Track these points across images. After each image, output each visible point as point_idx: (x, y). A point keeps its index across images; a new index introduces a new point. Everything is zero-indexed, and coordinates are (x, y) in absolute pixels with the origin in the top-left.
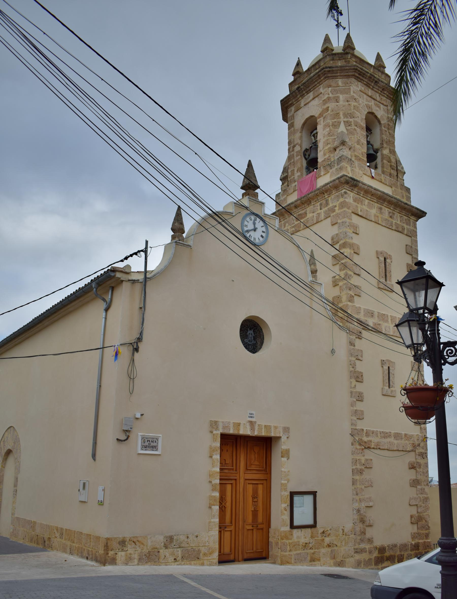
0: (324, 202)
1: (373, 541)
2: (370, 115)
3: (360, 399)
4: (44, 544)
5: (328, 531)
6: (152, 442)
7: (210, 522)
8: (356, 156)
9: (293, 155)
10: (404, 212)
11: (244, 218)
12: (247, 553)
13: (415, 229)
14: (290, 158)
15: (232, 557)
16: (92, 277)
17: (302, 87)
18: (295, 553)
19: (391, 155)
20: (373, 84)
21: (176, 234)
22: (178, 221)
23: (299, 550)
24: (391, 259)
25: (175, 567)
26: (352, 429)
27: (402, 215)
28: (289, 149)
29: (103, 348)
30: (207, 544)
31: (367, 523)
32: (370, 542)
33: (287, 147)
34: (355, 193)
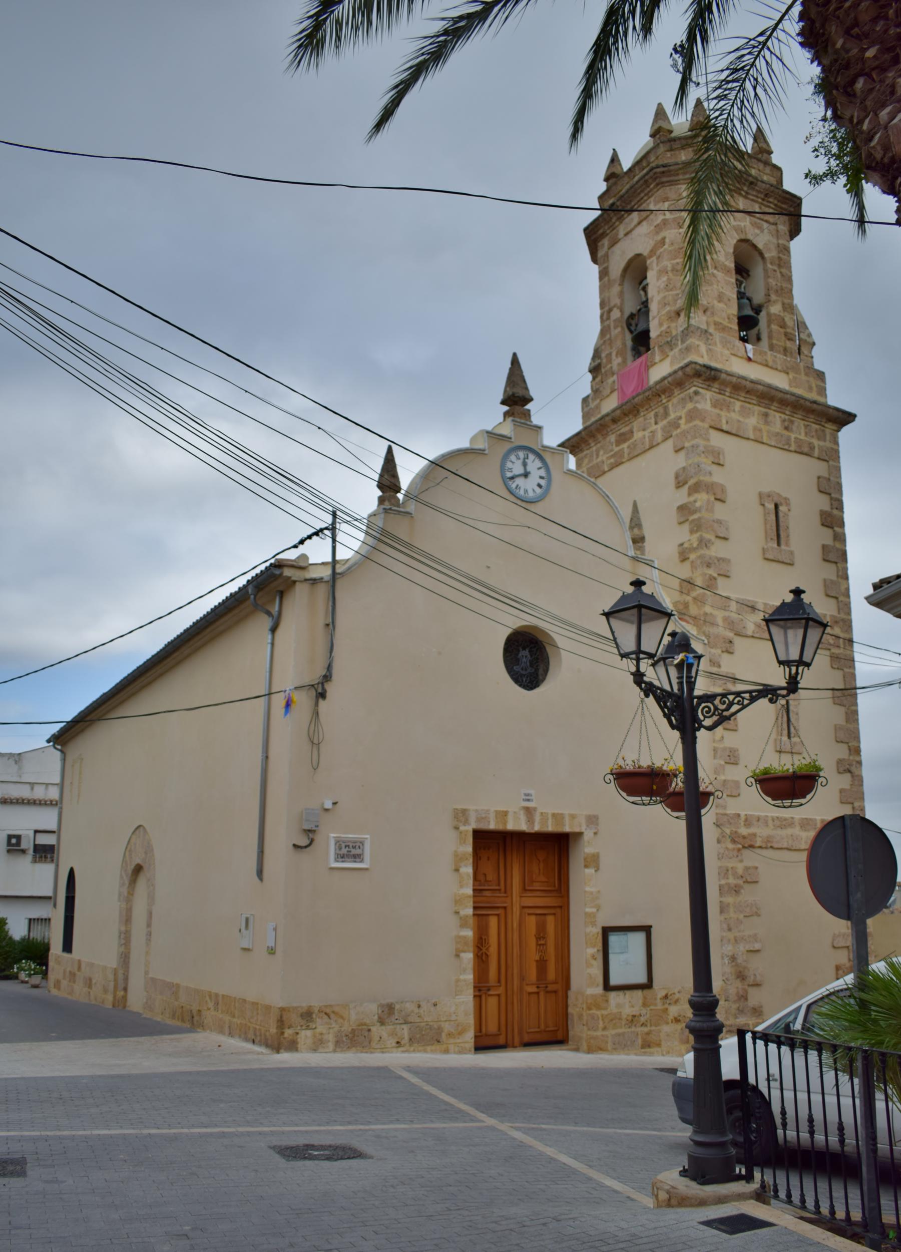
0: (660, 410)
1: (762, 1012)
2: (744, 245)
3: (732, 761)
4: (193, 1021)
5: (674, 994)
6: (354, 847)
7: (458, 981)
8: (716, 324)
9: (609, 326)
10: (812, 416)
11: (506, 457)
12: (528, 1033)
13: (835, 447)
14: (604, 332)
15: (502, 1040)
16: (249, 576)
17: (618, 203)
18: (613, 1032)
19: (786, 314)
20: (745, 188)
21: (385, 494)
22: (388, 471)
23: (621, 1027)
24: (788, 504)
25: (399, 1055)
26: (717, 814)
27: (808, 423)
28: (602, 316)
29: (270, 694)
30: (453, 1017)
31: (751, 980)
32: (757, 1014)
33: (598, 312)
34: (715, 392)
